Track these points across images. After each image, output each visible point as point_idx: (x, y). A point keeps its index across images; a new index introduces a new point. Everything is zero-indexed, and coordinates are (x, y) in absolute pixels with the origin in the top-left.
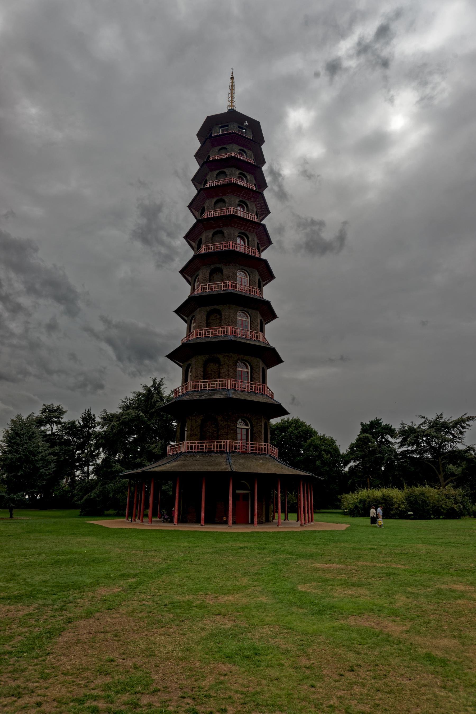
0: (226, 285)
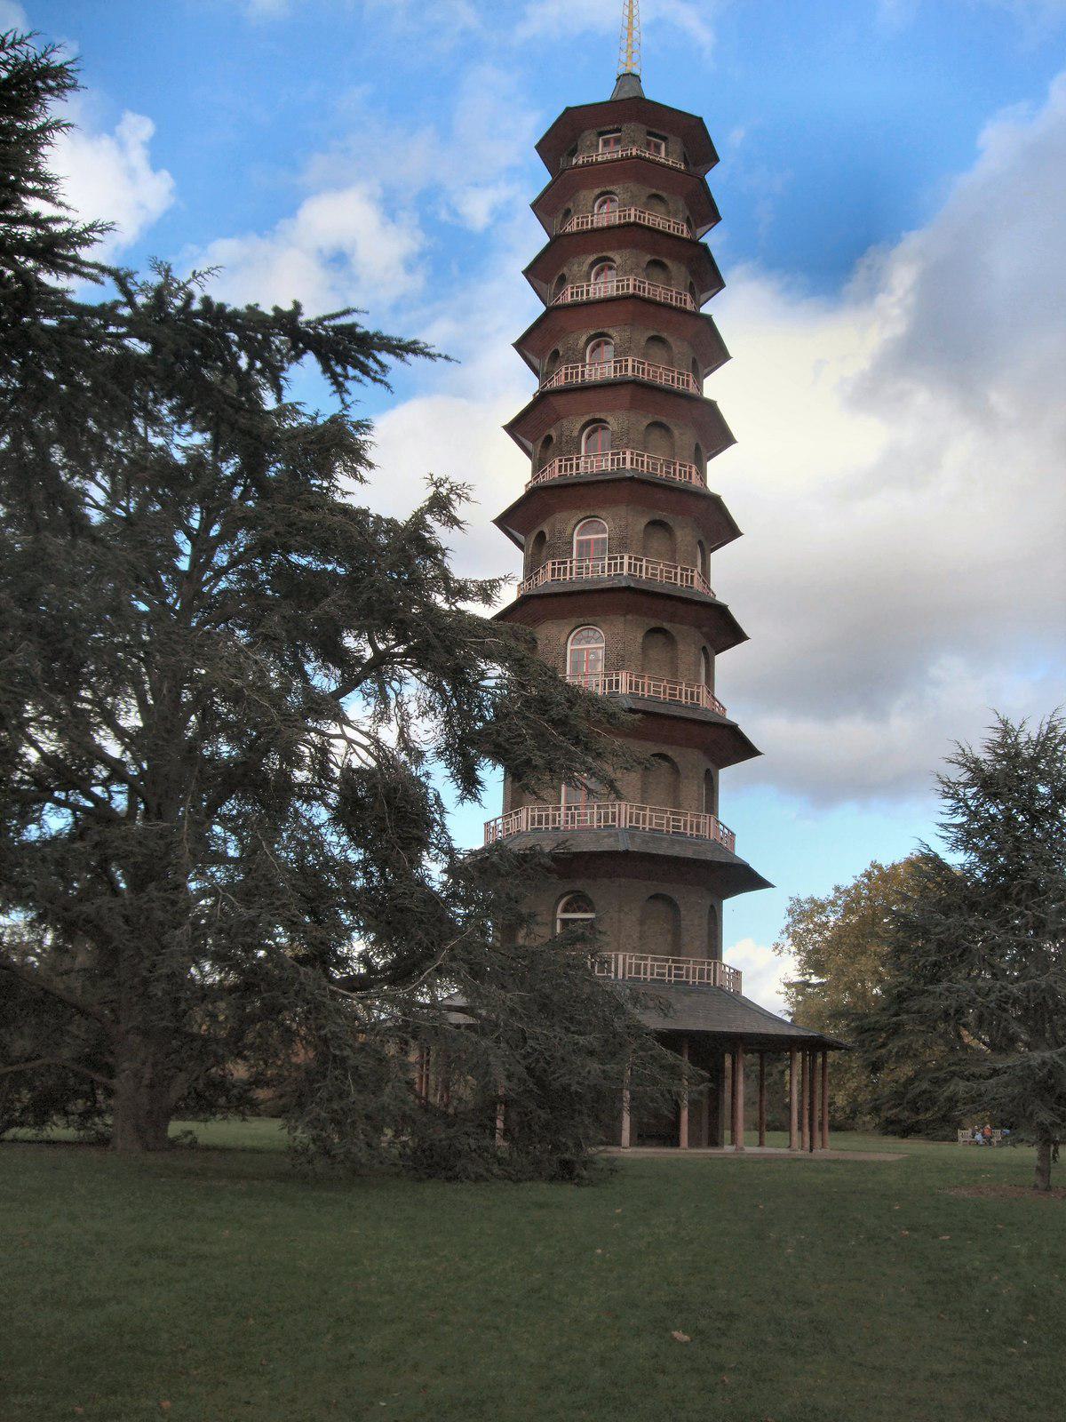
0: (623, 286)
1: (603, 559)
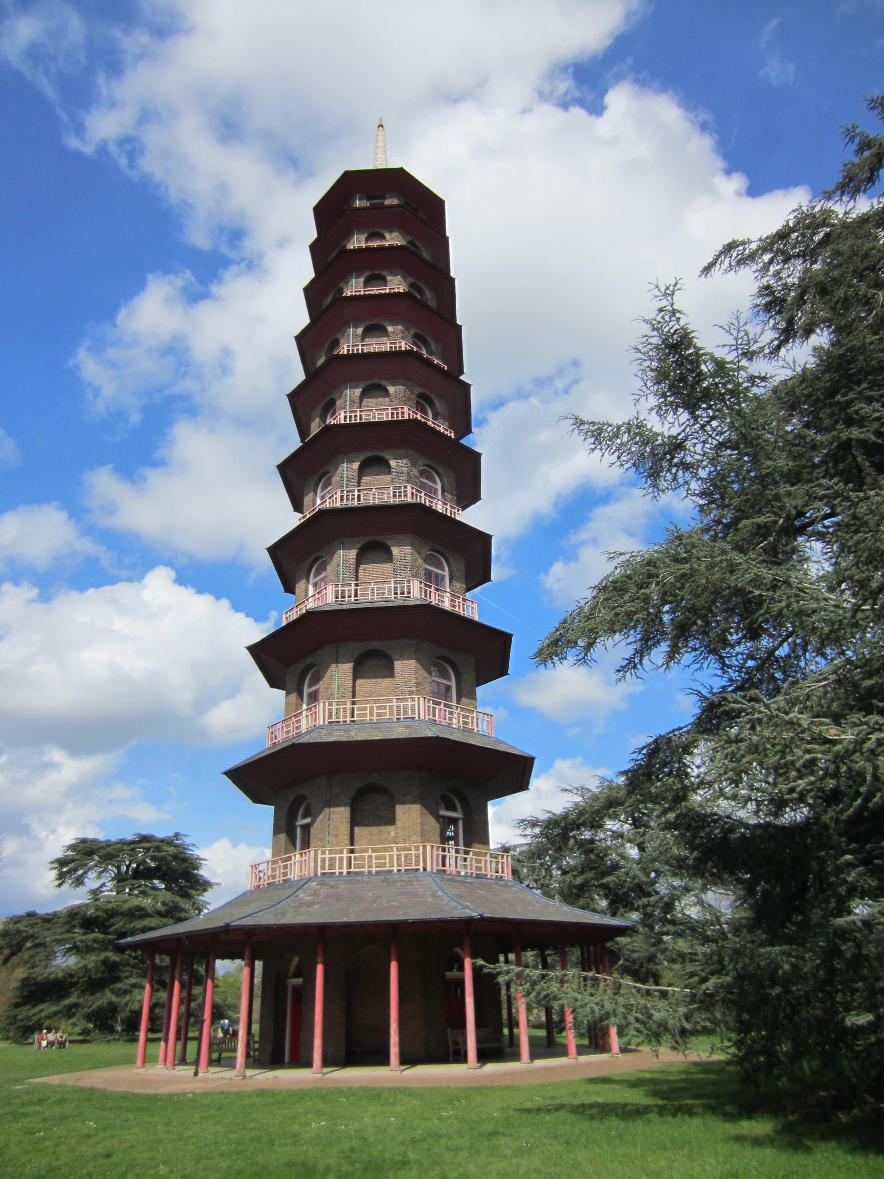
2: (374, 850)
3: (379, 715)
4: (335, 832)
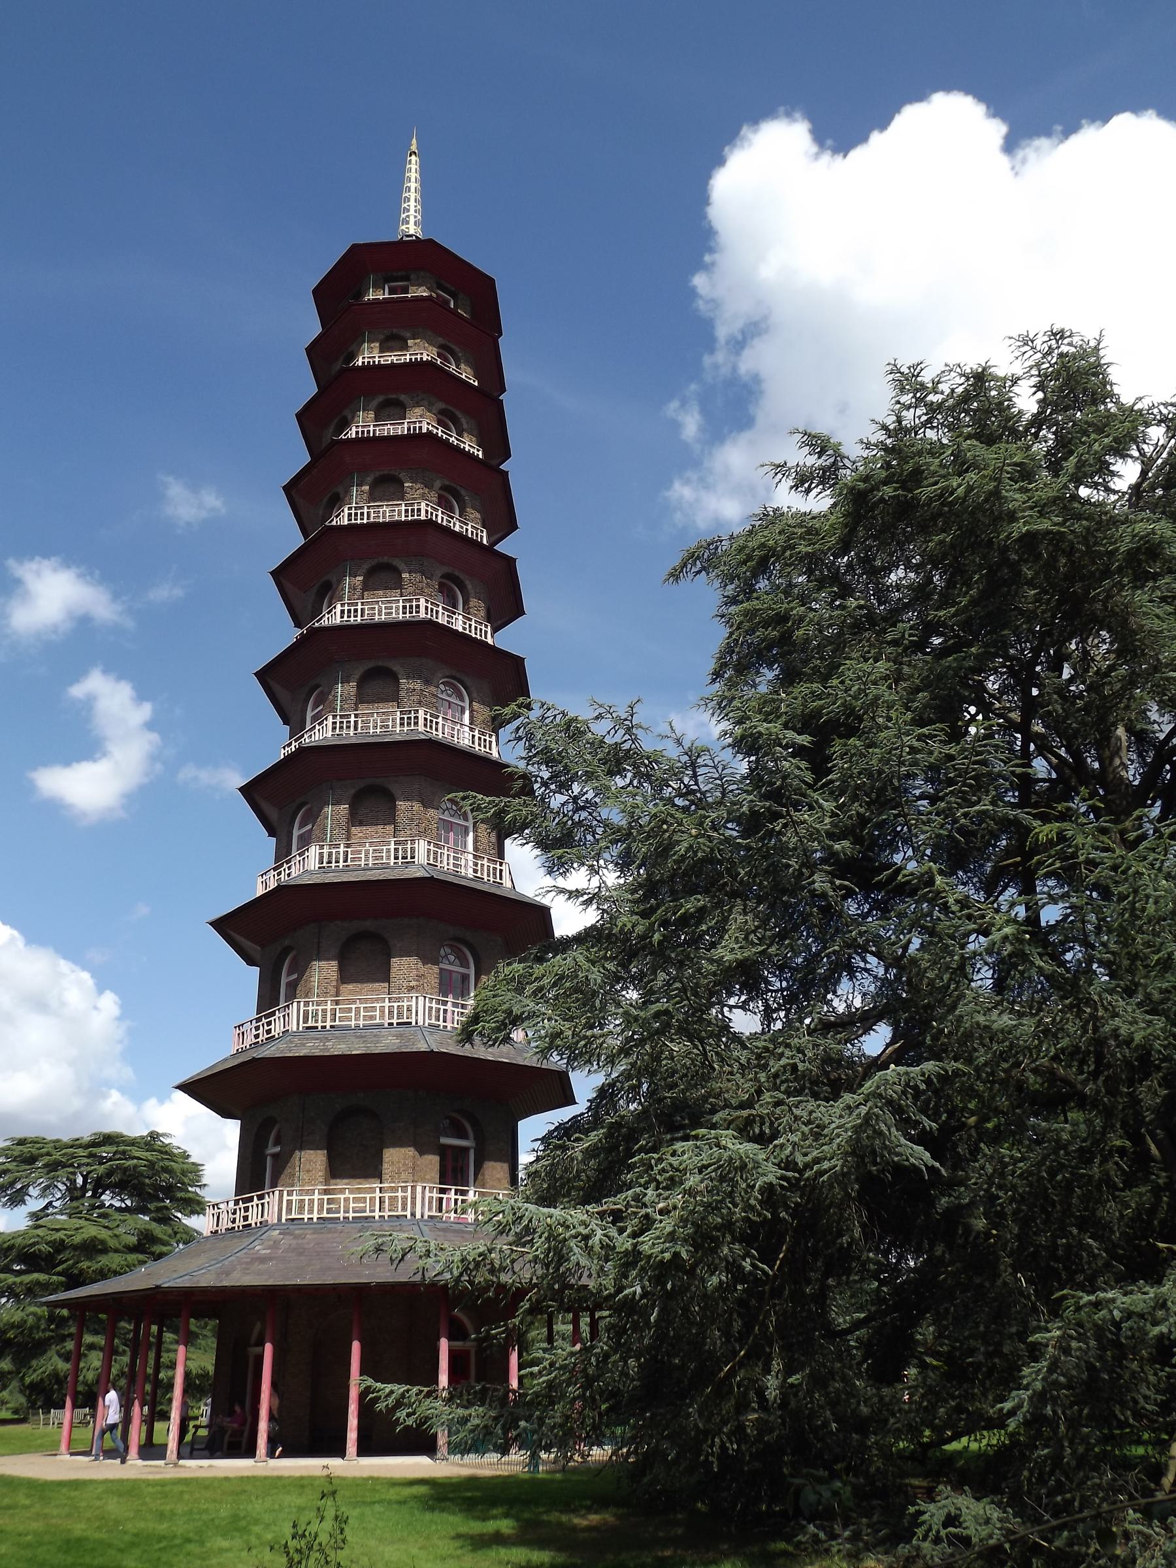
0: (413, 510)
1: (389, 843)
2: (351, 1192)
3: (376, 858)
4: (308, 1167)
